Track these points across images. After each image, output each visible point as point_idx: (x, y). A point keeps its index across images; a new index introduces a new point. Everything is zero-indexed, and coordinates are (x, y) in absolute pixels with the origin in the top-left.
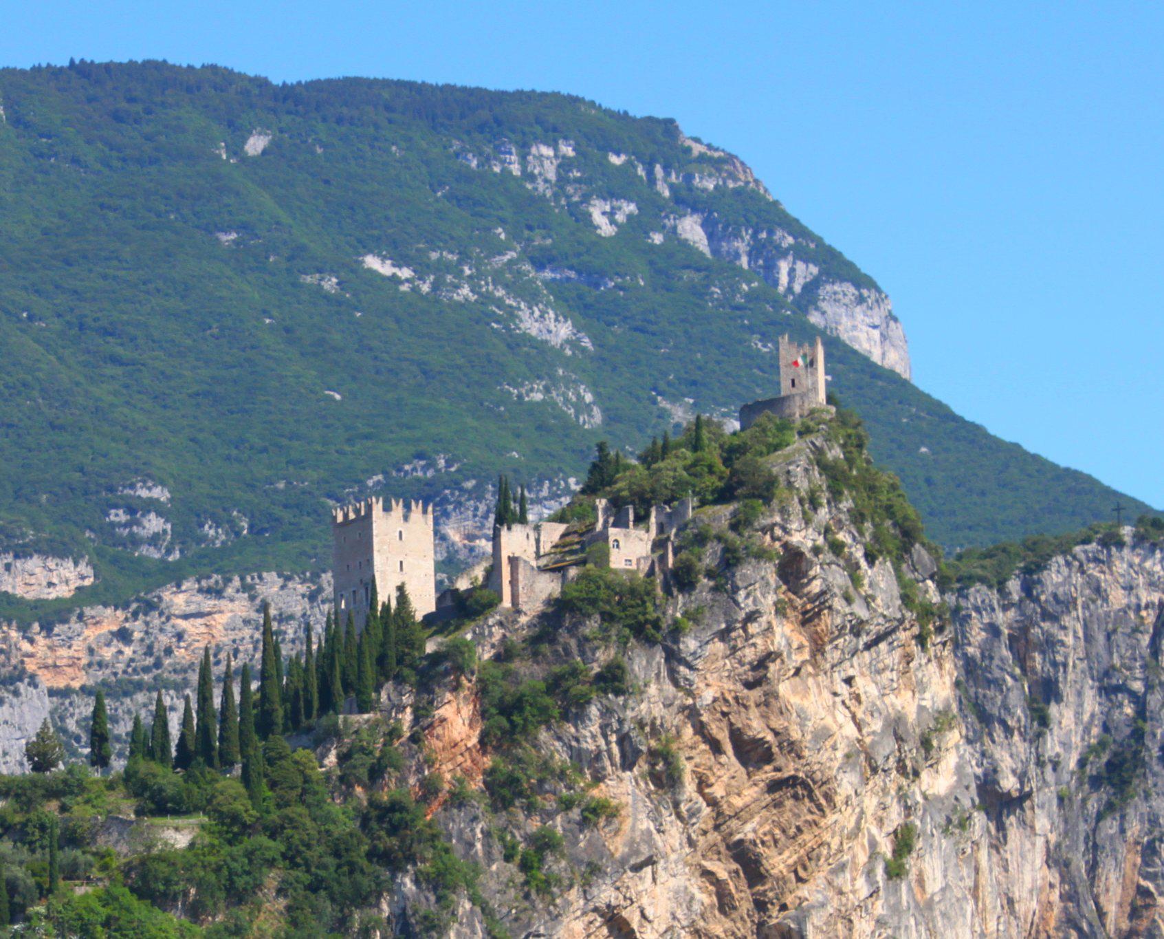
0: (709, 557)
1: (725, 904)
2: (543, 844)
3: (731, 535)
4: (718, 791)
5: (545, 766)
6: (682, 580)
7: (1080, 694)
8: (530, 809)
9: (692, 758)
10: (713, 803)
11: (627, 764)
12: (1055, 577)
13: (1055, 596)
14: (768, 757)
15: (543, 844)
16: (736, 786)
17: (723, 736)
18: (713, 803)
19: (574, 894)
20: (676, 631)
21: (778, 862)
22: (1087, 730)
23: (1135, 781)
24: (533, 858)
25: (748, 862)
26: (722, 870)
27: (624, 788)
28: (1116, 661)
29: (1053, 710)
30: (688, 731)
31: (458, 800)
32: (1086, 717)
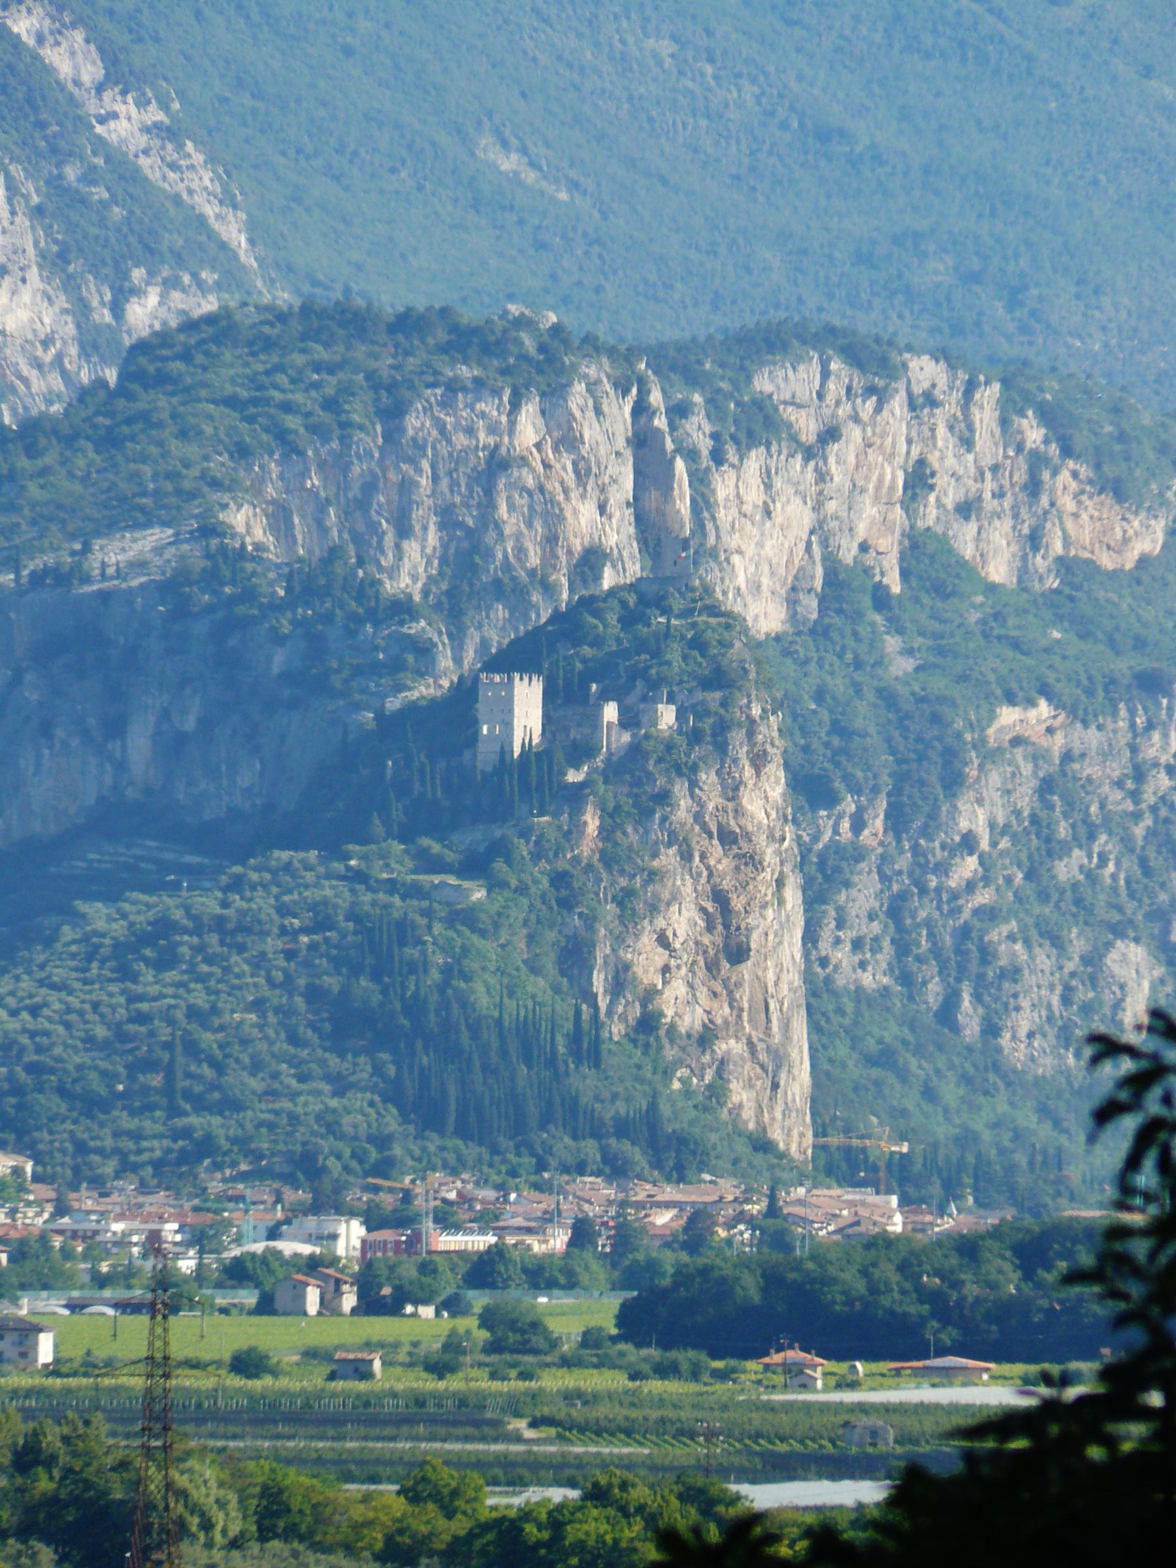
0: (707, 724)
1: (710, 928)
2: (629, 893)
3: (722, 711)
4: (712, 862)
5: (630, 848)
6: (695, 737)
7: (425, 528)
8: (622, 872)
9: (699, 842)
10: (708, 867)
11: (669, 845)
12: (415, 422)
13: (414, 439)
14: (735, 841)
15: (629, 893)
16: (720, 860)
17: (714, 829)
18: (708, 867)
19: (646, 922)
20: (694, 769)
21: (737, 903)
22: (429, 563)
23: (471, 613)
24: (624, 899)
25: (720, 897)
26: (710, 906)
27: (669, 858)
28: (457, 499)
29: (405, 544)
30: (697, 828)
31: (590, 867)
32: (429, 550)
